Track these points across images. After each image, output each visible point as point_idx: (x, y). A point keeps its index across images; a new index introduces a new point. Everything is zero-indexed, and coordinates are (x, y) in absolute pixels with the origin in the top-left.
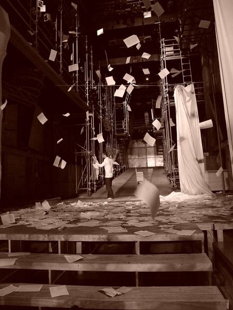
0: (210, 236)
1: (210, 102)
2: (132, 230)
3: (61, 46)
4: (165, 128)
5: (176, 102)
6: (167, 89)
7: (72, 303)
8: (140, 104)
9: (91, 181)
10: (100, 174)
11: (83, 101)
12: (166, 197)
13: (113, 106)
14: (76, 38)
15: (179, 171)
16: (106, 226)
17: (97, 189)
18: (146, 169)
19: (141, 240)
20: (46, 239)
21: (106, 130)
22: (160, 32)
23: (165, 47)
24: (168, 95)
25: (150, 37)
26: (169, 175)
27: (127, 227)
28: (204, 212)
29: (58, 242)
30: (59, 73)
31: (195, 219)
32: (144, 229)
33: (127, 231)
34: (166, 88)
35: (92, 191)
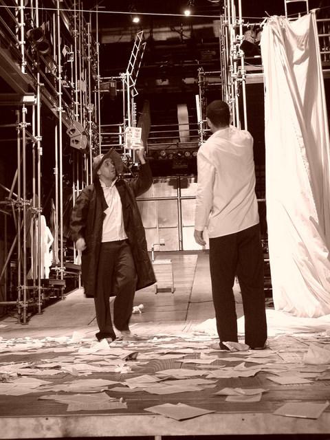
5: (265, 74)
6: (241, 37)
7: (199, 236)
8: (166, 83)
9: (30, 282)
11: (9, 59)
13: (94, 83)
16: (62, 393)
17: (47, 303)
18: (177, 257)
19: (165, 433)
21: (73, 145)
24: (242, 53)
27: (126, 396)
34: (237, 32)
35: (33, 311)
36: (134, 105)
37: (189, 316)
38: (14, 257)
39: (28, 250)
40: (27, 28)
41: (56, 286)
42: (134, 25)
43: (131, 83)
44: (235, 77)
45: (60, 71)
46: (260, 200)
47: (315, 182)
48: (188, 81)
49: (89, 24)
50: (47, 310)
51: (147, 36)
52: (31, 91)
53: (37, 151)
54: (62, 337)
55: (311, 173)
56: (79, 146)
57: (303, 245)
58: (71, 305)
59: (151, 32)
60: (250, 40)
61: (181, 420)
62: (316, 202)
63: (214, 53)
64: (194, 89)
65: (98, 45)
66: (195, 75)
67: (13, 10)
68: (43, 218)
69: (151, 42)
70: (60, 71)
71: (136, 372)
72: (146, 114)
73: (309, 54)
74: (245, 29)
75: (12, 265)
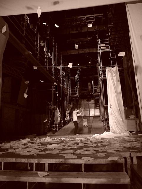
0: (129, 160)
1: (128, 77)
2: (80, 156)
3: (39, 43)
4: (100, 92)
6: (102, 69)
8: (85, 77)
9: (55, 124)
10: (60, 120)
16: (64, 153)
17: (59, 129)
18: (89, 117)
21: (65, 93)
22: (97, 36)
24: (102, 72)
28: (124, 145)
29: (33, 163)
30: (37, 59)
31: (119, 149)
34: (101, 68)
35: (56, 131)
37: (91, 132)
43: (77, 78)
44: (101, 77)
46: (83, 166)
48: (90, 77)
52: (56, 82)
53: (57, 95)
57: (116, 117)
58: (64, 129)
68: (58, 110)
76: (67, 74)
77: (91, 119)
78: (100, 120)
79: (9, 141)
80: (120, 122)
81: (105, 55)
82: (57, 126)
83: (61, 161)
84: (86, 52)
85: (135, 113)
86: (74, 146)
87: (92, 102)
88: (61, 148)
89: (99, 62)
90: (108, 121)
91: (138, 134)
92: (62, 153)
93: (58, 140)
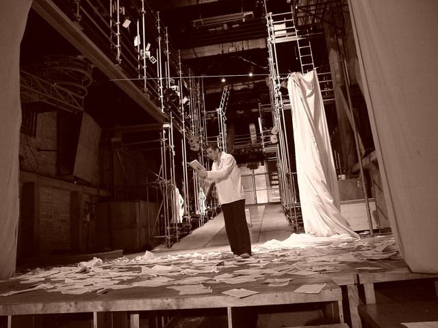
0: (353, 295)
1: (344, 100)
2: (219, 289)
3: (118, 22)
4: (279, 142)
5: (291, 104)
6: (279, 85)
8: (242, 112)
9: (172, 225)
11: (155, 107)
12: (283, 242)
13: (202, 115)
14: (142, 13)
15: (302, 207)
16: (179, 285)
17: (182, 236)
19: (233, 306)
20: (73, 310)
22: (265, 6)
23: (273, 24)
24: (280, 93)
25: (251, 13)
26: (287, 212)
27: (212, 286)
28: (341, 258)
29: (92, 313)
30: (116, 62)
31: (327, 268)
32: (238, 286)
33: (211, 291)
34: (277, 83)
35: (174, 241)
36: (225, 125)
38: (162, 212)
39: (170, 207)
40: (163, 89)
41: (186, 227)
42: (223, 83)
43: (222, 114)
44: (278, 105)
45: (183, 110)
47: (324, 162)
48: (254, 110)
49: (198, 84)
50: (181, 240)
51: (230, 88)
52: (168, 121)
54: (187, 254)
55: (320, 155)
56: (195, 150)
57: (318, 196)
59: (232, 86)
60: (284, 86)
61: (241, 298)
62: (324, 172)
63: (267, 94)
64: (257, 115)
65: (203, 95)
66: (257, 107)
67: (156, 80)
68: (177, 190)
69: (232, 91)
70: (183, 110)
71: (222, 272)
72: (232, 130)
73: (315, 91)
74: (281, 81)
75: (162, 216)
76: (197, 105)
77: (259, 209)
78: (281, 212)
79: (47, 265)
80: (328, 207)
81: (285, 50)
82: (177, 228)
83: (168, 305)
84: (241, 49)
85: (366, 185)
86: (210, 268)
87: (262, 169)
88: (176, 274)
89: (272, 70)
90: (299, 211)
91: (373, 236)
92: (174, 285)
93: (174, 258)
